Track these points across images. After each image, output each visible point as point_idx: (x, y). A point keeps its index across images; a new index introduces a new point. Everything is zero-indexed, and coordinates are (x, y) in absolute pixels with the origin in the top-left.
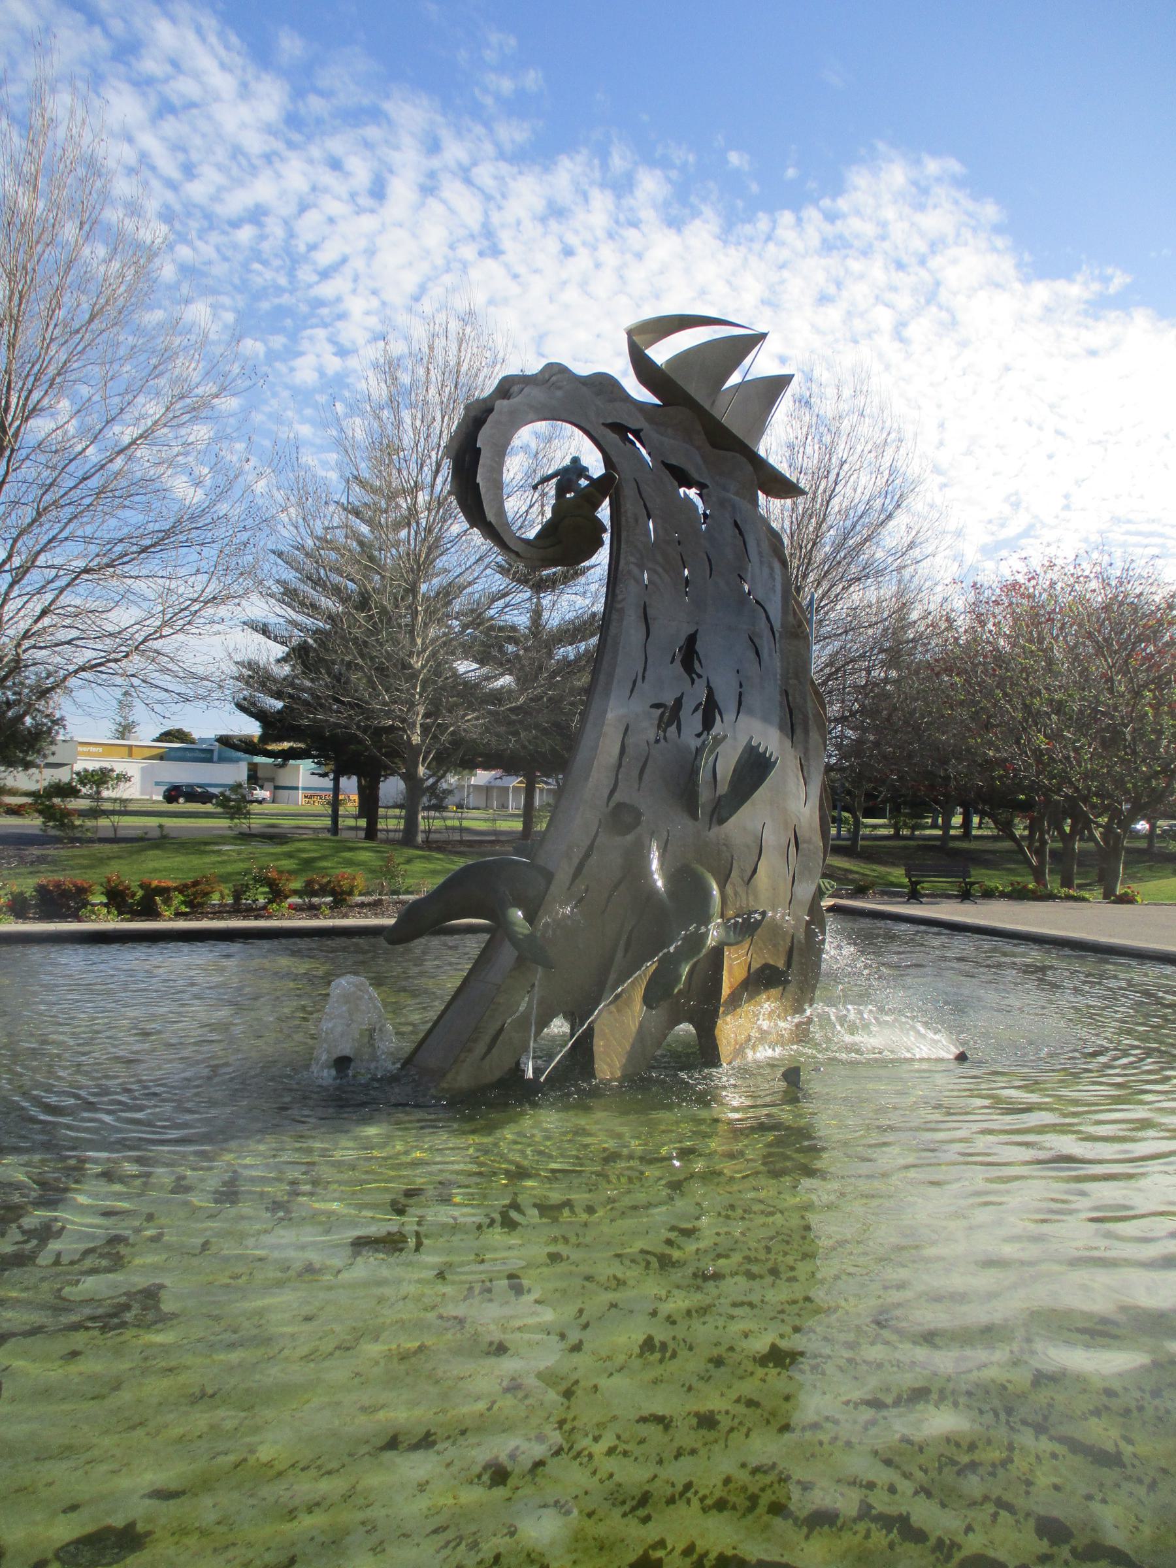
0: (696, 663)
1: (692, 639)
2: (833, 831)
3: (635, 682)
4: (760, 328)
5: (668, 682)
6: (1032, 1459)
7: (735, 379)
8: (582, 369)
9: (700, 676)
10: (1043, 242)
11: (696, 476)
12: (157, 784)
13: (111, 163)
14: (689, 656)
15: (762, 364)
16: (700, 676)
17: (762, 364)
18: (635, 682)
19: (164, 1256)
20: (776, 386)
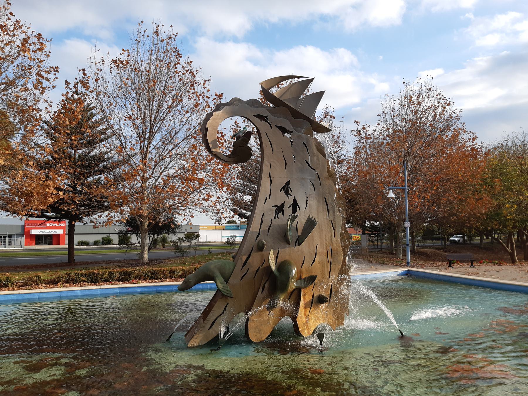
0: (290, 191)
1: (288, 183)
2: (256, 187)
3: (266, 199)
4: (309, 75)
5: (280, 198)
6: (28, 26)
7: (302, 96)
8: (245, 98)
9: (291, 195)
10: (305, 46)
11: (288, 129)
12: (80, 71)
13: (169, 240)
14: (286, 189)
15: (313, 89)
16: (291, 195)
17: (313, 89)
18: (266, 199)
19: (92, 154)
20: (319, 95)
